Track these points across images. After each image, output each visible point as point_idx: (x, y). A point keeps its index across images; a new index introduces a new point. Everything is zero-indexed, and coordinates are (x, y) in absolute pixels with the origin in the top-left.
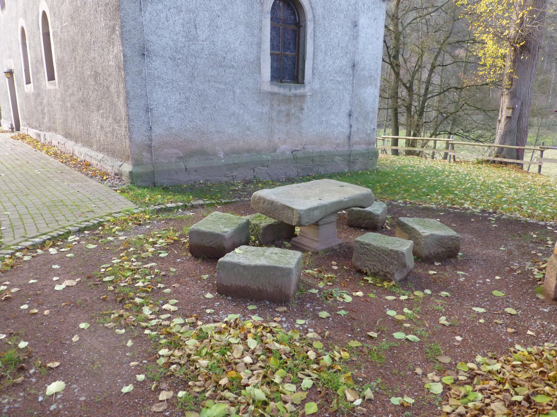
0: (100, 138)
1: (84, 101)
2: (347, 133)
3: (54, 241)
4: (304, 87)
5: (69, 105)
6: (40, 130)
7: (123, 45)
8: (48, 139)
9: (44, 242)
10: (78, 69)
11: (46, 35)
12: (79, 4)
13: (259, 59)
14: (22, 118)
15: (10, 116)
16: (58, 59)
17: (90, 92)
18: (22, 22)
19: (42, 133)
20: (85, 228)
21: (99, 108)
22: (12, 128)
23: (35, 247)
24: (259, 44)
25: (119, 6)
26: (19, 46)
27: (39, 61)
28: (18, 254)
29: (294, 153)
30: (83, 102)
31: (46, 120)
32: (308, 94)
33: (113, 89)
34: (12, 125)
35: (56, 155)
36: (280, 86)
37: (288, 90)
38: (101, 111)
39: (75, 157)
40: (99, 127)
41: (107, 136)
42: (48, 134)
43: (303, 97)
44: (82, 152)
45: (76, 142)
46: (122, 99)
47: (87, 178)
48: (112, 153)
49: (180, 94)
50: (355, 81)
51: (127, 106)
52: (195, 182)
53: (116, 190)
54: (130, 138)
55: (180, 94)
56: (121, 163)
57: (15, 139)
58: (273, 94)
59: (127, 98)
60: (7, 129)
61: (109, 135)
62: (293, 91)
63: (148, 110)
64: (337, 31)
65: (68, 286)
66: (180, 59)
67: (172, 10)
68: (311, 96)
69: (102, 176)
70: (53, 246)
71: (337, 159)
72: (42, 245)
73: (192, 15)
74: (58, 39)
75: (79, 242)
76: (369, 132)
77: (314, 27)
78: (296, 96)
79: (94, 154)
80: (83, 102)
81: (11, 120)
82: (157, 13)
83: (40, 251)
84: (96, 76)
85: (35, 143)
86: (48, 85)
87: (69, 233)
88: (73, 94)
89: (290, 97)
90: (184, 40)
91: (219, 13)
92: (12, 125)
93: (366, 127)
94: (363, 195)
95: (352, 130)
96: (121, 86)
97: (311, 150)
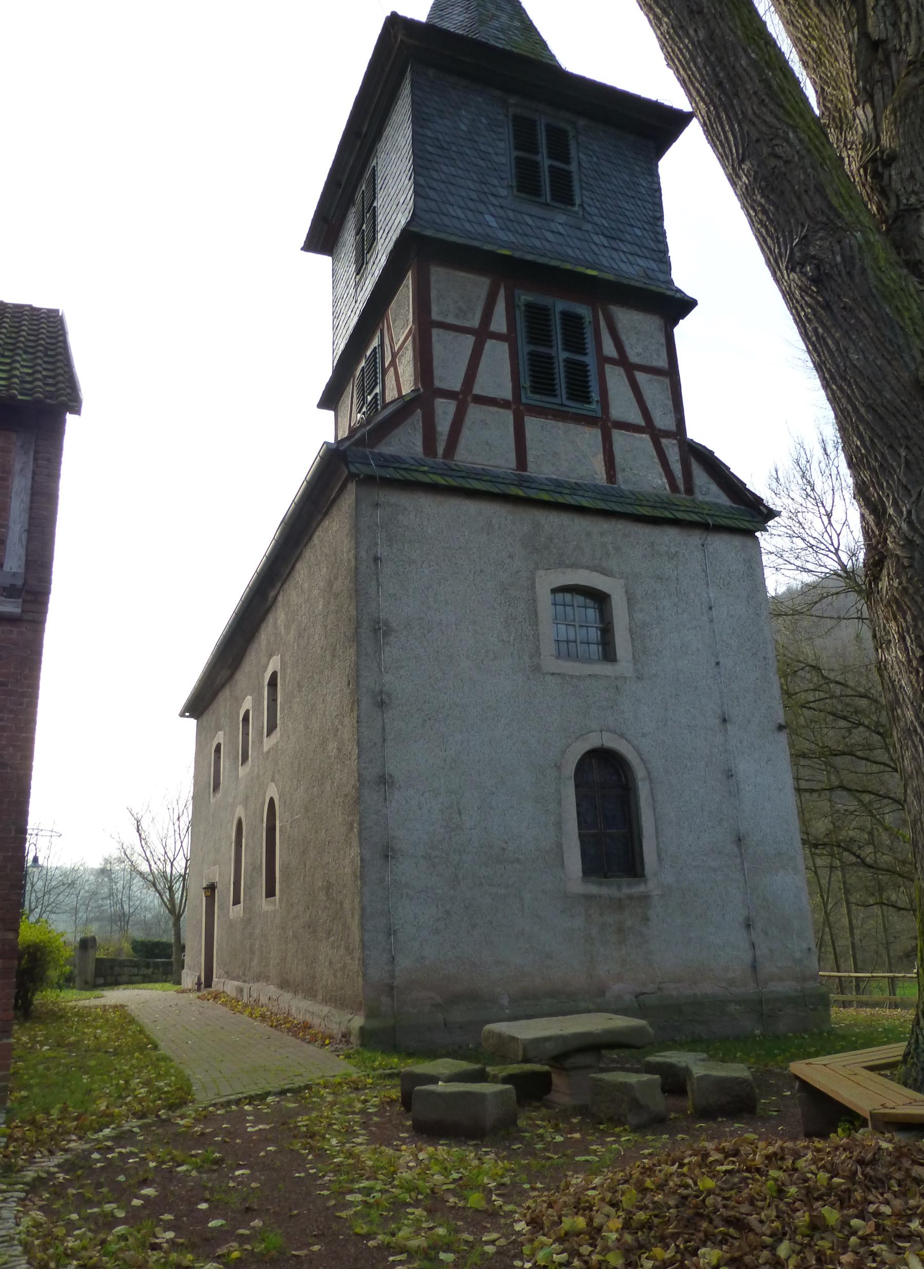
0: (327, 980)
1: (310, 926)
2: (748, 957)
3: (251, 1099)
4: (646, 882)
5: (291, 933)
6: (244, 982)
7: (360, 846)
8: (255, 995)
9: (240, 1100)
10: (307, 879)
11: (271, 830)
12: (316, 793)
13: (560, 845)
14: (218, 964)
15: (199, 963)
16: (282, 865)
17: (320, 912)
18: (240, 812)
19: (246, 986)
20: (289, 1090)
21: (329, 933)
22: (199, 984)
23: (229, 1103)
24: (559, 825)
25: (359, 798)
26: (231, 846)
27: (255, 868)
28: (211, 1109)
29: (642, 997)
30: (309, 927)
31: (255, 962)
32: (656, 893)
33: (347, 906)
34: (199, 978)
35: (263, 1017)
36: (600, 884)
37: (627, 889)
38: (332, 939)
39: (290, 1019)
40: (327, 964)
41: (336, 977)
42: (255, 986)
43: (645, 898)
44: (300, 1007)
45: (295, 993)
46: (357, 917)
47: (304, 1044)
48: (338, 1001)
49: (437, 906)
50: (746, 865)
51: (362, 927)
52: (460, 1047)
53: (338, 1056)
54: (364, 975)
55: (437, 906)
56: (350, 1016)
57: (203, 1000)
58: (588, 897)
59: (362, 917)
60: (190, 986)
61: (339, 974)
62: (626, 891)
63: (390, 932)
64: (696, 788)
65: (260, 1130)
66: (436, 857)
67: (426, 795)
68: (662, 896)
69: (320, 1039)
70: (249, 1104)
71: (733, 1008)
72: (238, 1102)
73: (453, 796)
74: (286, 837)
75: (278, 1102)
76: (798, 955)
77: (652, 789)
78: (630, 897)
79: (316, 1007)
80: (309, 927)
81: (200, 969)
82: (407, 802)
83: (234, 1107)
84: (328, 887)
85: (233, 1004)
86: (265, 905)
87: (268, 1094)
88: (297, 917)
89: (620, 900)
90: (443, 830)
91: (494, 789)
92: (199, 978)
93: (790, 946)
94: (628, 1027)
95: (758, 953)
96: (357, 900)
97: (675, 993)
